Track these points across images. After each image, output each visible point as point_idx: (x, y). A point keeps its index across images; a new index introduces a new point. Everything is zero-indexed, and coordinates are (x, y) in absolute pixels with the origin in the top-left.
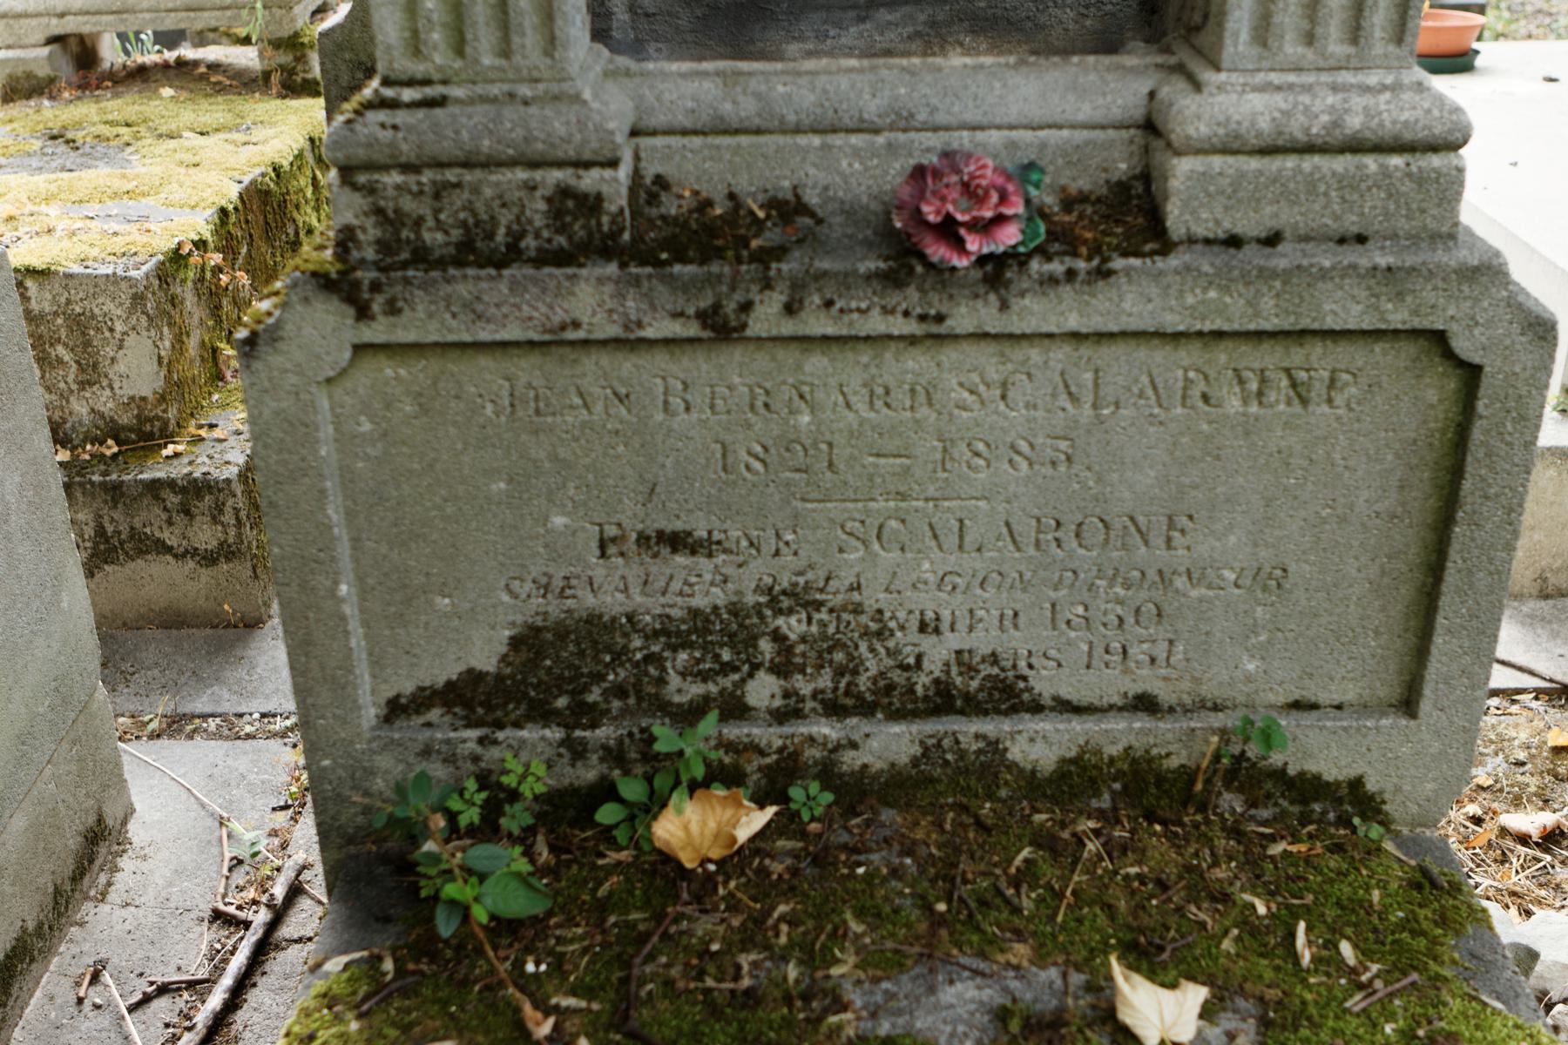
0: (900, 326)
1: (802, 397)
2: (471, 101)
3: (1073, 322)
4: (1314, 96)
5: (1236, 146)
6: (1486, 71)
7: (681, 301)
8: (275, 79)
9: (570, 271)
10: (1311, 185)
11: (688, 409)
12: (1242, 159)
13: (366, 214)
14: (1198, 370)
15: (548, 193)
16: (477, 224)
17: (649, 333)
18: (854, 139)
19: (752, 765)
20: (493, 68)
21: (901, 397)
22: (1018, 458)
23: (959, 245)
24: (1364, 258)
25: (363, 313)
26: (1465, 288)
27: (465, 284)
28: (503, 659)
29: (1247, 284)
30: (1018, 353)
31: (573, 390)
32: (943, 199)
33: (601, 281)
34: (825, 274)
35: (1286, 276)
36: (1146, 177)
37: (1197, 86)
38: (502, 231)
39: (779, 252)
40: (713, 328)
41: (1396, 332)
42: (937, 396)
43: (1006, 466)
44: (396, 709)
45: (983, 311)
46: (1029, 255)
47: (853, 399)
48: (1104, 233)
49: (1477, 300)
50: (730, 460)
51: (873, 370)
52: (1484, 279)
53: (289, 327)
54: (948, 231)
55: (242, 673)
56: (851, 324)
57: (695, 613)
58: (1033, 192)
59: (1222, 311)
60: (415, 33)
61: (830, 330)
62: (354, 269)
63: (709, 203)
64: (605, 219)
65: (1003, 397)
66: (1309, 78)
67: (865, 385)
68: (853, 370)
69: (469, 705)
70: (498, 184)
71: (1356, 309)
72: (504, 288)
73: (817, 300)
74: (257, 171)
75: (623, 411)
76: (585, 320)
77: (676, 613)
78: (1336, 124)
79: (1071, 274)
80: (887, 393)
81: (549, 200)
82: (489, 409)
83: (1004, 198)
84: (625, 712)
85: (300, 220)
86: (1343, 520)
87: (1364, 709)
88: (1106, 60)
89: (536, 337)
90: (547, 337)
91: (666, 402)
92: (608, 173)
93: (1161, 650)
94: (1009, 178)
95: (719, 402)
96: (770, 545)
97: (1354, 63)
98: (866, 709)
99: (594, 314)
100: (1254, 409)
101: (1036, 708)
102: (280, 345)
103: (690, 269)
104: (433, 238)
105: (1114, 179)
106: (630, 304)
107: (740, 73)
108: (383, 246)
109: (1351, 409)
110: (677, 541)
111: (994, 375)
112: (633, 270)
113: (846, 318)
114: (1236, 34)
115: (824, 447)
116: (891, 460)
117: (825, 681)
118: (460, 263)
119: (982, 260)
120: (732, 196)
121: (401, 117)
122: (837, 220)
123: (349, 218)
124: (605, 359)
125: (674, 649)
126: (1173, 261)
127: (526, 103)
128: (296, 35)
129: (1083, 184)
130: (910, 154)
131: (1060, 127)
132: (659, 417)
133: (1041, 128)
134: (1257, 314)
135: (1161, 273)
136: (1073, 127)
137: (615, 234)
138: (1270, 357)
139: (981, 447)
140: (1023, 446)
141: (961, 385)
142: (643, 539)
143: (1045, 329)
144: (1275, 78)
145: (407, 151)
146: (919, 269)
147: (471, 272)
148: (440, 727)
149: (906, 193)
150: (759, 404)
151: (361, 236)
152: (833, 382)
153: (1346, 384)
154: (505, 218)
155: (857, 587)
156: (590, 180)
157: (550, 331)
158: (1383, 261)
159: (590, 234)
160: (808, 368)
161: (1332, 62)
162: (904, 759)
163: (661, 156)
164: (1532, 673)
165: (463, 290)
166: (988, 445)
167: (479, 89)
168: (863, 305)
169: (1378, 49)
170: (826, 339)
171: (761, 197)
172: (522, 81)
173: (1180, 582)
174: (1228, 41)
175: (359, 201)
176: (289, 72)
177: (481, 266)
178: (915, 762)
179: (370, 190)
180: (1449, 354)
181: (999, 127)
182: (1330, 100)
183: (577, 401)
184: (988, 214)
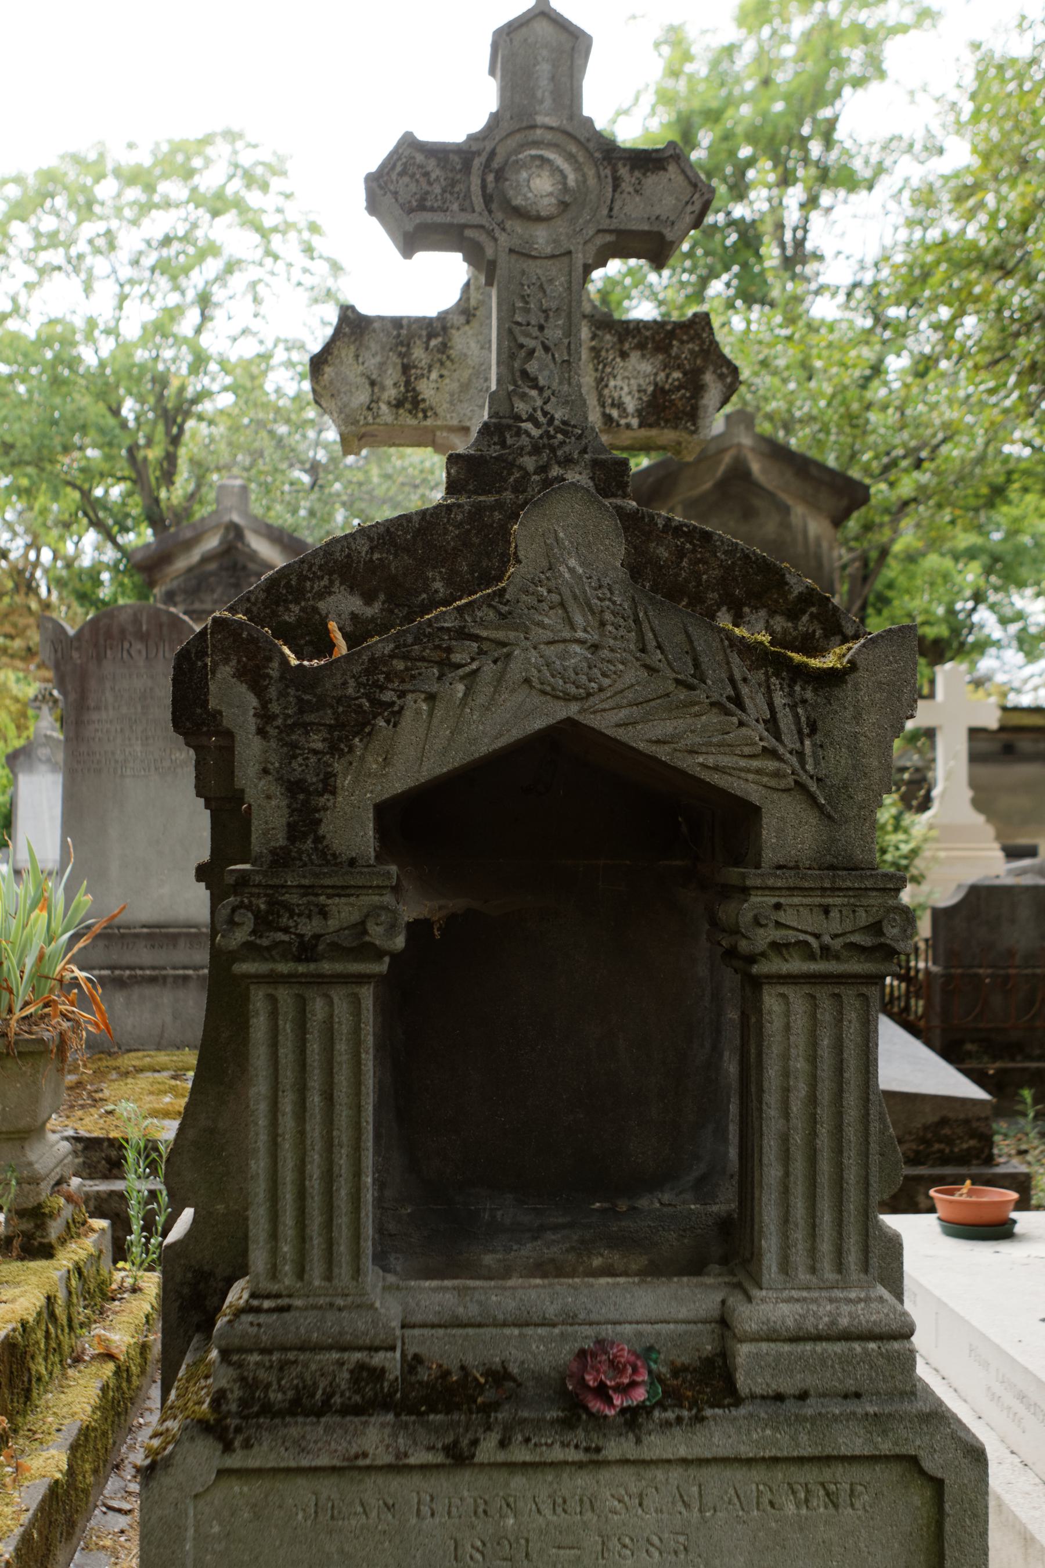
0: (573, 1455)
1: (508, 1505)
2: (306, 1308)
3: (682, 1452)
4: (819, 1305)
5: (774, 1336)
7: (433, 1438)
8: (16, 1243)
9: (364, 1419)
10: (823, 1361)
11: (433, 1515)
12: (779, 1344)
13: (235, 1381)
14: (765, 1484)
15: (351, 1367)
16: (304, 1388)
17: (412, 1461)
18: (540, 1331)
20: (319, 1287)
21: (573, 1505)
22: (652, 1549)
25: (228, 1448)
26: (924, 1426)
29: (789, 1425)
30: (649, 1473)
31: (357, 1501)
32: (598, 1371)
33: (383, 1425)
34: (525, 1420)
35: (813, 1420)
37: (749, 1299)
38: (320, 1392)
39: (494, 1406)
40: (453, 1458)
41: (886, 1457)
42: (597, 1505)
43: (645, 1555)
45: (625, 1445)
46: (653, 1407)
47: (542, 1507)
48: (699, 1392)
49: (932, 1435)
50: (460, 1552)
51: (555, 1486)
52: (935, 1421)
53: (178, 1457)
54: (602, 1392)
56: (541, 1454)
58: (653, 1366)
60: (274, 1266)
61: (528, 1459)
62: (225, 1418)
63: (447, 1373)
64: (386, 1384)
65: (641, 1505)
66: (815, 1294)
67: (549, 1496)
68: (541, 1486)
70: (320, 1361)
71: (859, 1442)
72: (321, 1430)
73: (520, 1438)
74: (10, 1327)
75: (390, 1517)
76: (371, 1452)
78: (833, 1323)
79: (679, 1420)
80: (565, 1502)
81: (352, 1372)
82: (300, 1516)
83: (635, 1371)
85: (33, 1367)
88: (695, 1280)
89: (337, 1462)
90: (345, 1464)
91: (418, 1510)
92: (389, 1355)
94: (638, 1357)
95: (454, 1510)
97: (841, 1284)
99: (377, 1448)
100: (804, 1511)
102: (170, 1470)
103: (439, 1417)
105: (704, 1356)
106: (401, 1440)
107: (467, 1288)
108: (243, 1403)
109: (866, 1511)
111: (634, 1490)
112: (404, 1418)
113: (538, 1450)
114: (769, 1268)
115: (523, 1542)
116: (568, 1551)
118: (294, 1414)
119: (623, 1411)
120: (463, 1368)
121: (262, 1318)
122: (531, 1384)
123: (223, 1383)
124: (380, 1479)
126: (743, 1411)
127: (340, 1309)
128: (40, 1206)
129: (685, 1359)
130: (576, 1341)
131: (669, 1322)
132: (414, 1521)
133: (656, 1323)
134: (798, 1445)
135: (735, 1419)
136: (676, 1322)
137: (391, 1394)
138: (810, 1475)
139: (627, 1541)
140: (655, 1540)
141: (613, 1496)
143: (665, 1456)
144: (794, 1294)
145: (265, 1339)
146: (584, 1417)
147: (300, 1419)
149: (575, 1367)
150: (480, 1510)
151: (230, 1396)
152: (529, 1495)
153: (861, 1493)
156: (378, 1359)
157: (348, 1459)
158: (871, 1409)
159: (376, 1395)
160: (513, 1485)
161: (828, 1284)
163: (419, 1342)
165: (294, 1432)
166: (632, 1540)
167: (311, 1300)
168: (549, 1441)
169: (854, 1277)
170: (525, 1465)
171: (481, 1368)
172: (337, 1295)
174: (765, 1272)
175: (232, 1373)
176: (28, 1236)
177: (307, 1416)
179: (240, 1365)
180: (922, 1472)
181: (630, 1323)
182: (828, 1308)
183: (359, 1509)
184: (626, 1381)
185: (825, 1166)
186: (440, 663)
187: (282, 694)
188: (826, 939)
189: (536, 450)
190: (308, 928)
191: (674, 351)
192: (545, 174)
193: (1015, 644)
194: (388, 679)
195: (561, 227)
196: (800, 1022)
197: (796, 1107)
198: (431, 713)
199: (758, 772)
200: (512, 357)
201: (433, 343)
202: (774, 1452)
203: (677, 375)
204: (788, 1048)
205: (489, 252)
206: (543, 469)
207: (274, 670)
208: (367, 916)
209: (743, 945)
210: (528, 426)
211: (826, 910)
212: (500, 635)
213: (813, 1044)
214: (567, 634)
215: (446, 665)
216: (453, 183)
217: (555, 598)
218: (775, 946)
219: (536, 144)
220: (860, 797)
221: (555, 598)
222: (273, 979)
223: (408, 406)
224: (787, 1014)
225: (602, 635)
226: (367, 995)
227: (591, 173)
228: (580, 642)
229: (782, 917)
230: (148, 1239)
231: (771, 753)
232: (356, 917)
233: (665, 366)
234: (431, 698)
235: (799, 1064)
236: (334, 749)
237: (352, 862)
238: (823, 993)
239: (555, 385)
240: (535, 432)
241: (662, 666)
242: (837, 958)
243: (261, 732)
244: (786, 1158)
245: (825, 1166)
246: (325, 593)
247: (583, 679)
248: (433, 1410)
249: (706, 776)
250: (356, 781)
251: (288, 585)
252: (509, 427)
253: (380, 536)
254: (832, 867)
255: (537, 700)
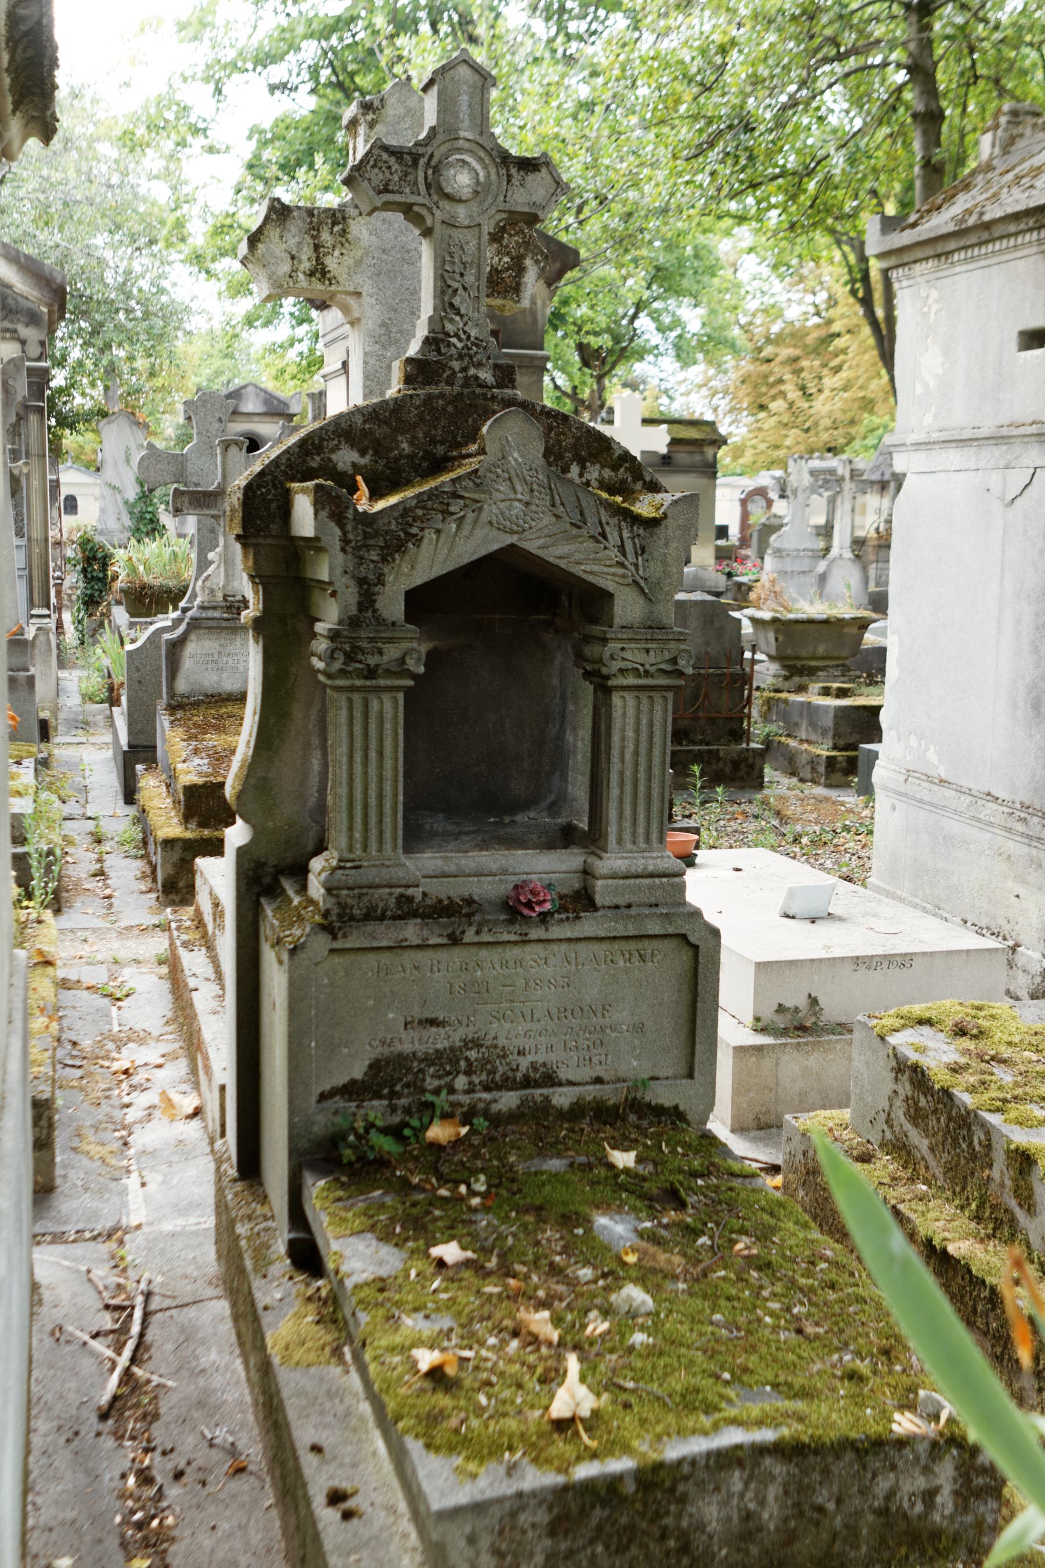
0: (513, 938)
3: (569, 935)
6: (700, 866)
10: (639, 888)
17: (431, 942)
19: (459, 1111)
21: (511, 964)
23: (533, 909)
24: (658, 911)
25: (335, 938)
27: (371, 927)
28: (365, 1074)
35: (635, 917)
36: (585, 888)
44: (323, 1097)
53: (309, 944)
54: (529, 905)
55: (54, 1213)
57: (437, 1051)
59: (616, 929)
61: (491, 940)
69: (351, 1094)
77: (431, 1051)
79: (568, 918)
84: (409, 1094)
86: (661, 1004)
87: (675, 1078)
93: (603, 1058)
96: (465, 1023)
98: (499, 1088)
101: (560, 1084)
104: (356, 912)
108: (340, 916)
110: (433, 1022)
111: (542, 955)
117: (484, 1077)
119: (540, 914)
121: (347, 872)
125: (429, 1066)
126: (600, 913)
129: (565, 891)
137: (417, 910)
138: (631, 946)
142: (420, 1022)
145: (351, 882)
148: (338, 1102)
154: (381, 905)
155: (495, 1038)
156: (410, 892)
162: (514, 1106)
164: (757, 1161)
170: (488, 943)
173: (608, 1031)
175: (333, 900)
178: (518, 1107)
179: (337, 896)
185: (642, 788)
186: (443, 512)
187: (355, 528)
188: (647, 667)
189: (460, 357)
190: (372, 661)
191: (505, 242)
192: (466, 172)
193: (672, 352)
194: (414, 520)
195: (474, 207)
196: (631, 712)
197: (628, 756)
198: (437, 540)
199: (613, 575)
200: (443, 293)
201: (336, 229)
202: (615, 934)
203: (506, 259)
204: (624, 725)
205: (429, 222)
206: (464, 370)
207: (350, 514)
208: (405, 654)
209: (604, 670)
210: (454, 340)
211: (648, 651)
212: (476, 496)
213: (638, 723)
214: (512, 496)
215: (446, 513)
216: (406, 174)
217: (506, 475)
218: (621, 670)
219: (459, 150)
220: (666, 589)
221: (506, 475)
222: (352, 689)
223: (318, 275)
224: (625, 707)
225: (532, 497)
226: (401, 696)
227: (493, 171)
228: (520, 501)
229: (625, 655)
230: (46, 883)
231: (621, 565)
232: (398, 654)
233: (499, 253)
234: (438, 532)
235: (630, 734)
236: (384, 560)
237: (394, 624)
238: (644, 696)
239: (470, 314)
240: (460, 345)
241: (564, 515)
242: (652, 677)
243: (343, 550)
244: (622, 784)
245: (642, 788)
246: (336, 449)
247: (521, 522)
248: (440, 916)
249: (585, 576)
250: (396, 578)
251: (313, 443)
252: (443, 341)
253: (370, 414)
254: (650, 627)
255: (494, 533)
